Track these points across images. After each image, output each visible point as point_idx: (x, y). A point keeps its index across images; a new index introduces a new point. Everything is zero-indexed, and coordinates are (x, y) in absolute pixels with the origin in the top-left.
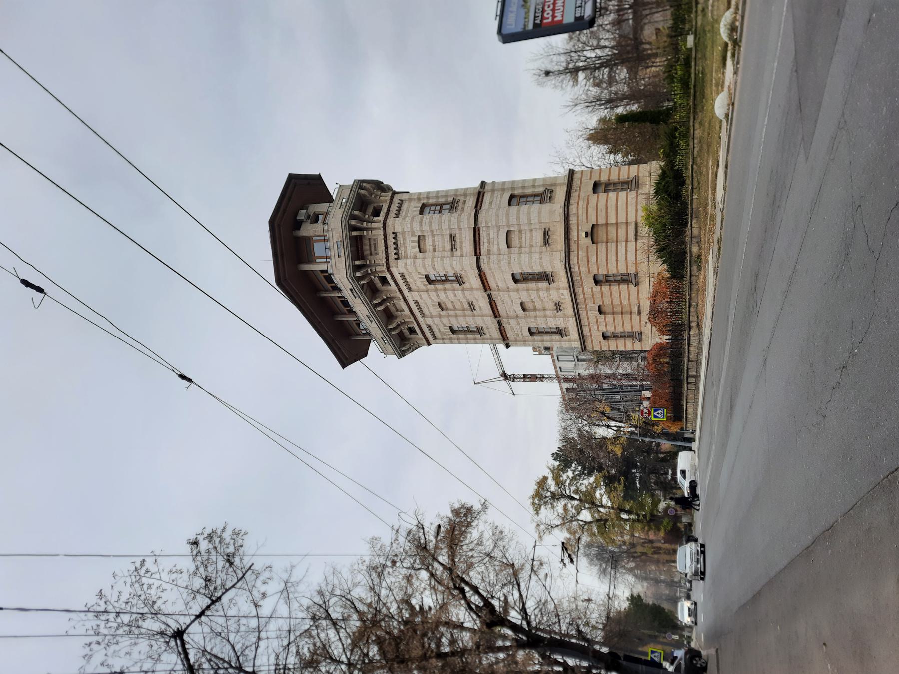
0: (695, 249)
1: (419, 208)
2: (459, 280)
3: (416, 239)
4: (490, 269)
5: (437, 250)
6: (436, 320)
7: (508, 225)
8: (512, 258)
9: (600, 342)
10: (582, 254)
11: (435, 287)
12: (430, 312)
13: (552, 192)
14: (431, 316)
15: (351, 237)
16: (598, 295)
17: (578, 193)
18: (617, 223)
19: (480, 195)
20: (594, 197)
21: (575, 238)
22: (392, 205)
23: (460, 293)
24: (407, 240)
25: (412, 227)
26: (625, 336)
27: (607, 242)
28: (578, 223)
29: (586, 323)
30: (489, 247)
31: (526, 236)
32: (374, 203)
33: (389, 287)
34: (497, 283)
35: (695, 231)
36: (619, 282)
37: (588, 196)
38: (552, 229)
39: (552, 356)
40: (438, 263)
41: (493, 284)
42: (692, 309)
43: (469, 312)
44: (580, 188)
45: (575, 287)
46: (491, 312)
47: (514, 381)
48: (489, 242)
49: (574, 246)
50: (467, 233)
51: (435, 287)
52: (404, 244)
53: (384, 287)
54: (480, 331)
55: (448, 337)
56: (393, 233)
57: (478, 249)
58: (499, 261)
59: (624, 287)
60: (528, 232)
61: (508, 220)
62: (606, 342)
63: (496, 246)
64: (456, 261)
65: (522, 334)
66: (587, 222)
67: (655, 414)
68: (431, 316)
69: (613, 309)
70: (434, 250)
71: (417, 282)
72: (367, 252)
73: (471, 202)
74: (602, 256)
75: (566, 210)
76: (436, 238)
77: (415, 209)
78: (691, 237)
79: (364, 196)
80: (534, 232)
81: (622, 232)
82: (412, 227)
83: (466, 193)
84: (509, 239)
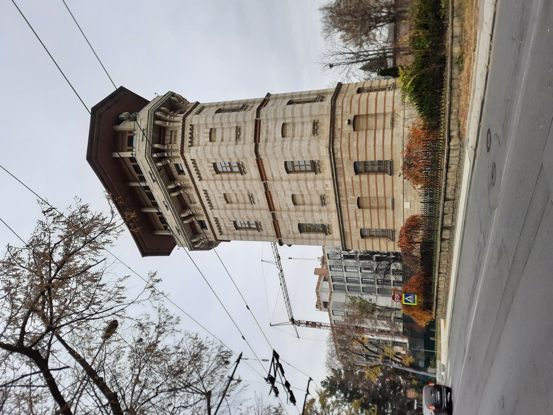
0: (456, 50)
2: (258, 227)
3: (208, 131)
4: (266, 155)
5: (224, 139)
6: (222, 212)
7: (284, 118)
8: (285, 145)
9: (358, 240)
10: (344, 140)
11: (221, 177)
12: (217, 205)
13: (323, 97)
14: (218, 209)
15: (155, 125)
16: (357, 186)
18: (376, 114)
19: (264, 102)
21: (339, 127)
23: (241, 183)
24: (201, 131)
25: (206, 120)
26: (380, 236)
28: (342, 114)
29: (347, 219)
30: (267, 136)
31: (298, 128)
32: (182, 109)
33: (184, 176)
34: (272, 173)
35: (457, 31)
36: (379, 237)
38: (320, 121)
39: (329, 311)
40: (223, 150)
41: (268, 174)
42: (453, 117)
43: (249, 206)
45: (338, 176)
46: (268, 206)
47: (299, 325)
48: (267, 132)
49: (338, 133)
50: (250, 126)
51: (221, 177)
52: (198, 135)
53: (180, 176)
54: (258, 227)
55: (232, 233)
56: (191, 125)
57: (258, 138)
58: (274, 147)
59: (380, 177)
60: (300, 125)
61: (284, 114)
62: (364, 240)
63: (272, 136)
64: (239, 148)
65: (293, 231)
66: (350, 113)
67: (406, 298)
68: (218, 209)
69: (370, 204)
70: (222, 140)
71: (206, 170)
72: (167, 141)
74: (362, 142)
75: (333, 102)
76: (225, 131)
78: (452, 37)
80: (305, 124)
81: (380, 122)
82: (206, 120)
83: (254, 102)
84: (284, 130)
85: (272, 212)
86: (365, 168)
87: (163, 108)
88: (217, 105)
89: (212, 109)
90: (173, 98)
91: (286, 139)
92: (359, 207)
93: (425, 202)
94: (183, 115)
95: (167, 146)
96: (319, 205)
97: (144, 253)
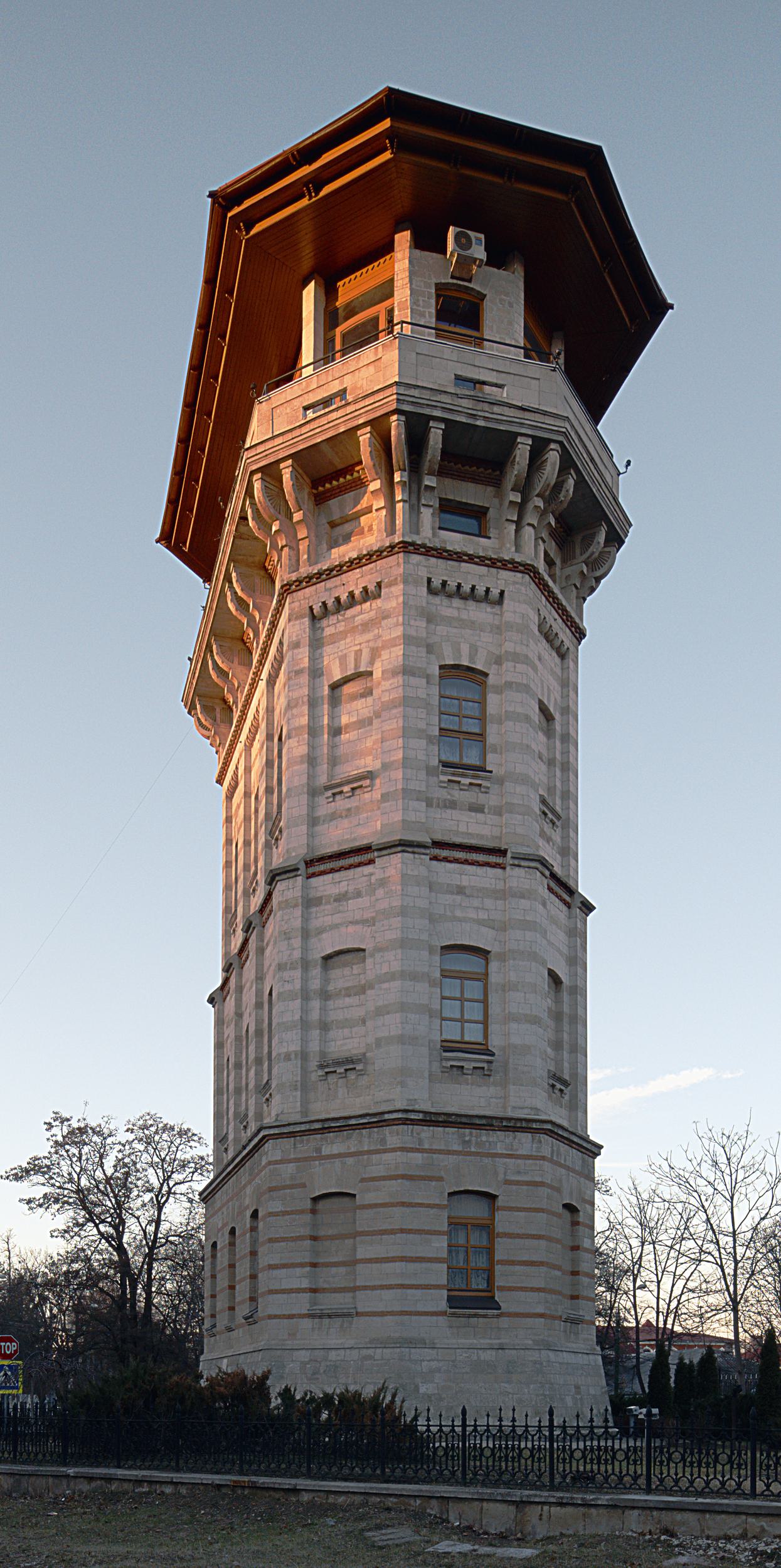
8: (292, 973)
15: (509, 440)
20: (433, 1193)
21: (326, 1150)
22: (483, 570)
27: (314, 1238)
37: (440, 1179)
38: (363, 1081)
49: (306, 1146)
57: (322, 868)
66: (363, 1180)
73: (473, 829)
77: (465, 648)
79: (589, 540)
83: (569, 852)
85: (302, 866)
87: (571, 482)
88: (569, 712)
89: (555, 686)
90: (602, 537)
93: (551, 1427)
94: (541, 566)
95: (432, 488)
96: (323, 1054)
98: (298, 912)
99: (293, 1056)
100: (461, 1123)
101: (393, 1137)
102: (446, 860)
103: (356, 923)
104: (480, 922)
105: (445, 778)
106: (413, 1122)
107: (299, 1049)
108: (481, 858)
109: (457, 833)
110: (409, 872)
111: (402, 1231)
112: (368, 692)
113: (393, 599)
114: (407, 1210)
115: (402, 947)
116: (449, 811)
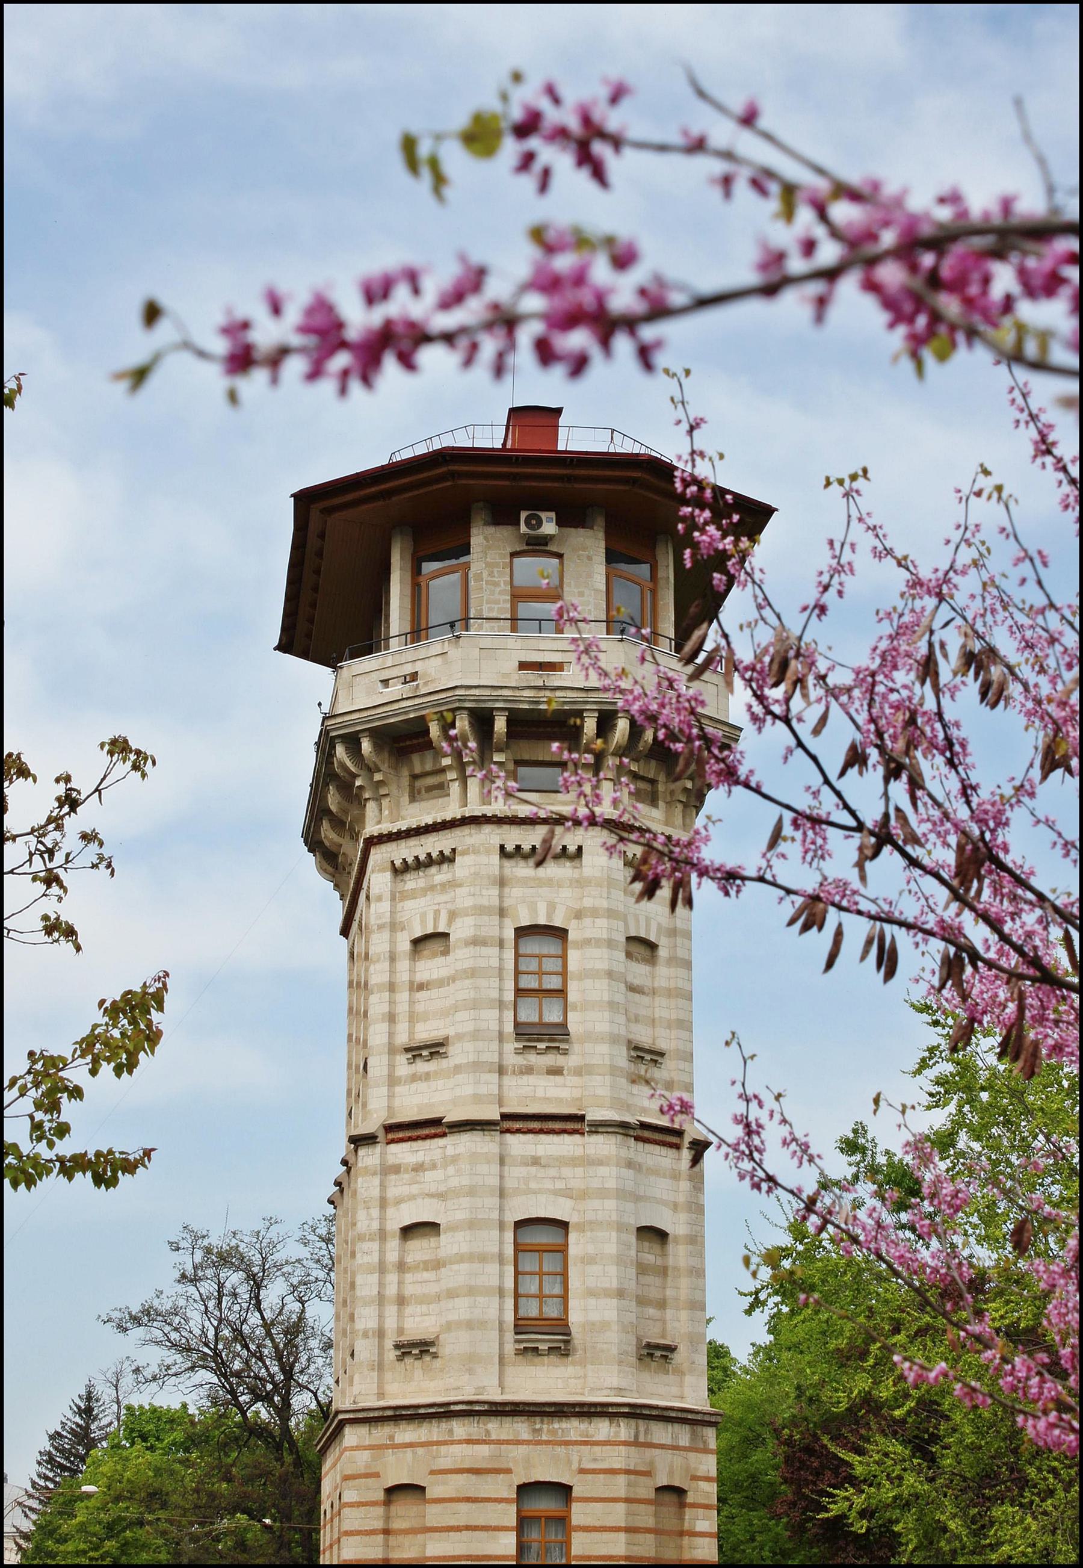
1: (542, 921)
3: (557, 923)
17: (525, 1436)
27: (386, 1532)
37: (508, 1471)
38: (438, 1363)
44: (548, 1443)
48: (419, 1168)
49: (381, 1433)
52: (432, 888)
57: (401, 1135)
66: (433, 1472)
73: (553, 1093)
85: (381, 1135)
86: (539, 1518)
91: (633, 1239)
92: (391, 1491)
96: (401, 1331)
97: (305, 500)
98: (376, 1181)
99: (370, 1333)
100: (529, 1411)
101: (460, 1428)
102: (518, 1131)
103: (431, 1196)
104: (557, 1193)
105: (520, 1045)
106: (479, 1413)
107: (376, 1326)
108: (558, 1126)
109: (534, 1099)
110: (479, 1150)
111: (468, 1528)
112: (446, 952)
113: (463, 866)
114: (474, 1506)
115: (470, 1228)
116: (525, 1077)
